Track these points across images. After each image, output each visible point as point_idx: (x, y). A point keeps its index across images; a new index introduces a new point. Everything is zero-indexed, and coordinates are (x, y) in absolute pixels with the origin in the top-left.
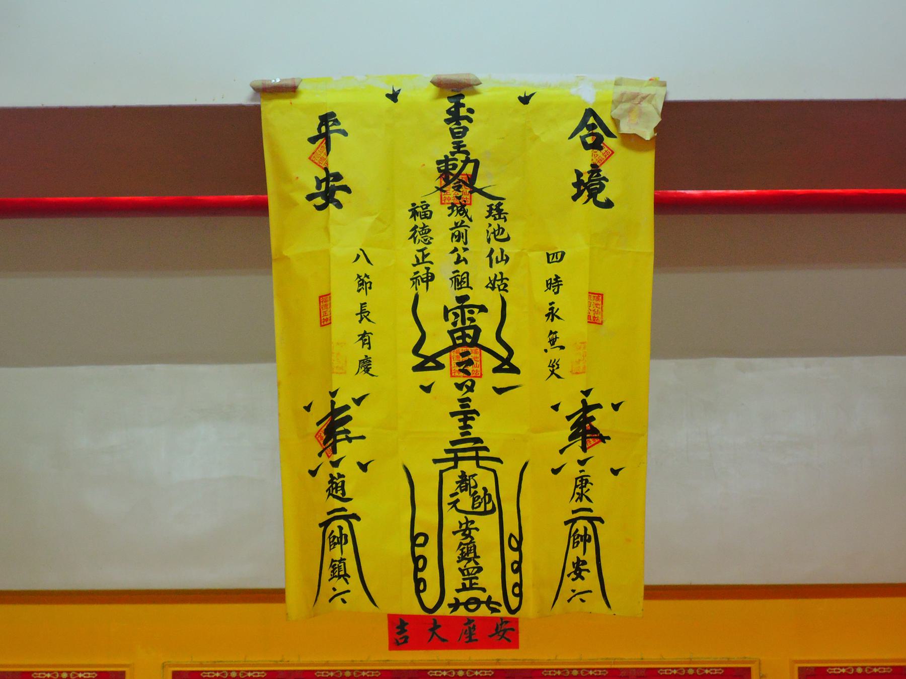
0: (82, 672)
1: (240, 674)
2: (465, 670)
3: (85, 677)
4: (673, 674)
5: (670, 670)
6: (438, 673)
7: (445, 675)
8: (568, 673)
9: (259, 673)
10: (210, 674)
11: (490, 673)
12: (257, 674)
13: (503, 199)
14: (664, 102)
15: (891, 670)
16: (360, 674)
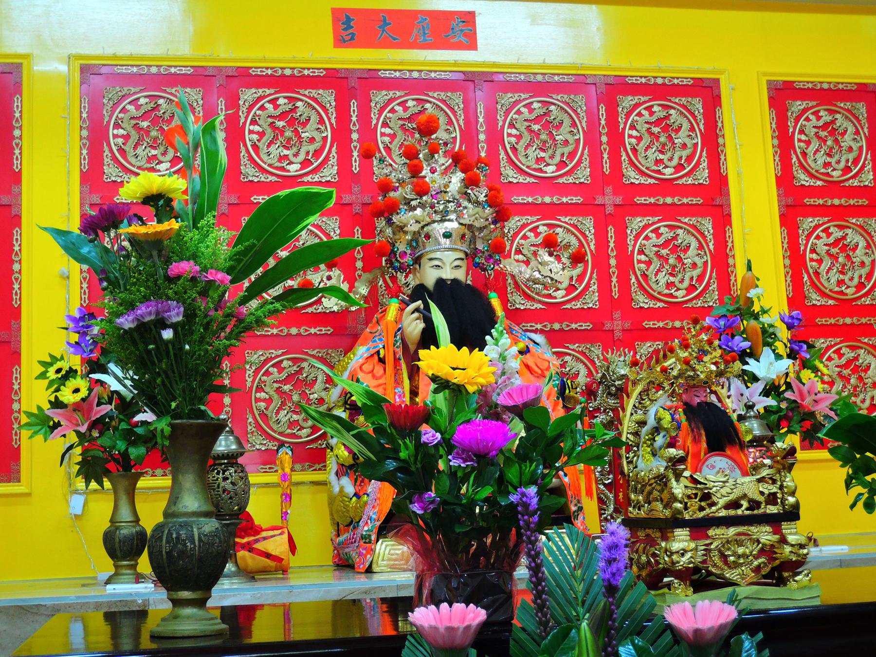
0: (175, 67)
1: (774, 135)
2: (159, 66)
3: (353, 159)
4: (567, 197)
5: (264, 70)
6: (85, 159)
7: (269, 73)
8: (85, 275)
9: (184, 69)
10: (729, 236)
11: (17, 167)
12: (85, 107)
13: (758, 72)
14: (81, 68)
15: (16, 306)
16: (302, 72)
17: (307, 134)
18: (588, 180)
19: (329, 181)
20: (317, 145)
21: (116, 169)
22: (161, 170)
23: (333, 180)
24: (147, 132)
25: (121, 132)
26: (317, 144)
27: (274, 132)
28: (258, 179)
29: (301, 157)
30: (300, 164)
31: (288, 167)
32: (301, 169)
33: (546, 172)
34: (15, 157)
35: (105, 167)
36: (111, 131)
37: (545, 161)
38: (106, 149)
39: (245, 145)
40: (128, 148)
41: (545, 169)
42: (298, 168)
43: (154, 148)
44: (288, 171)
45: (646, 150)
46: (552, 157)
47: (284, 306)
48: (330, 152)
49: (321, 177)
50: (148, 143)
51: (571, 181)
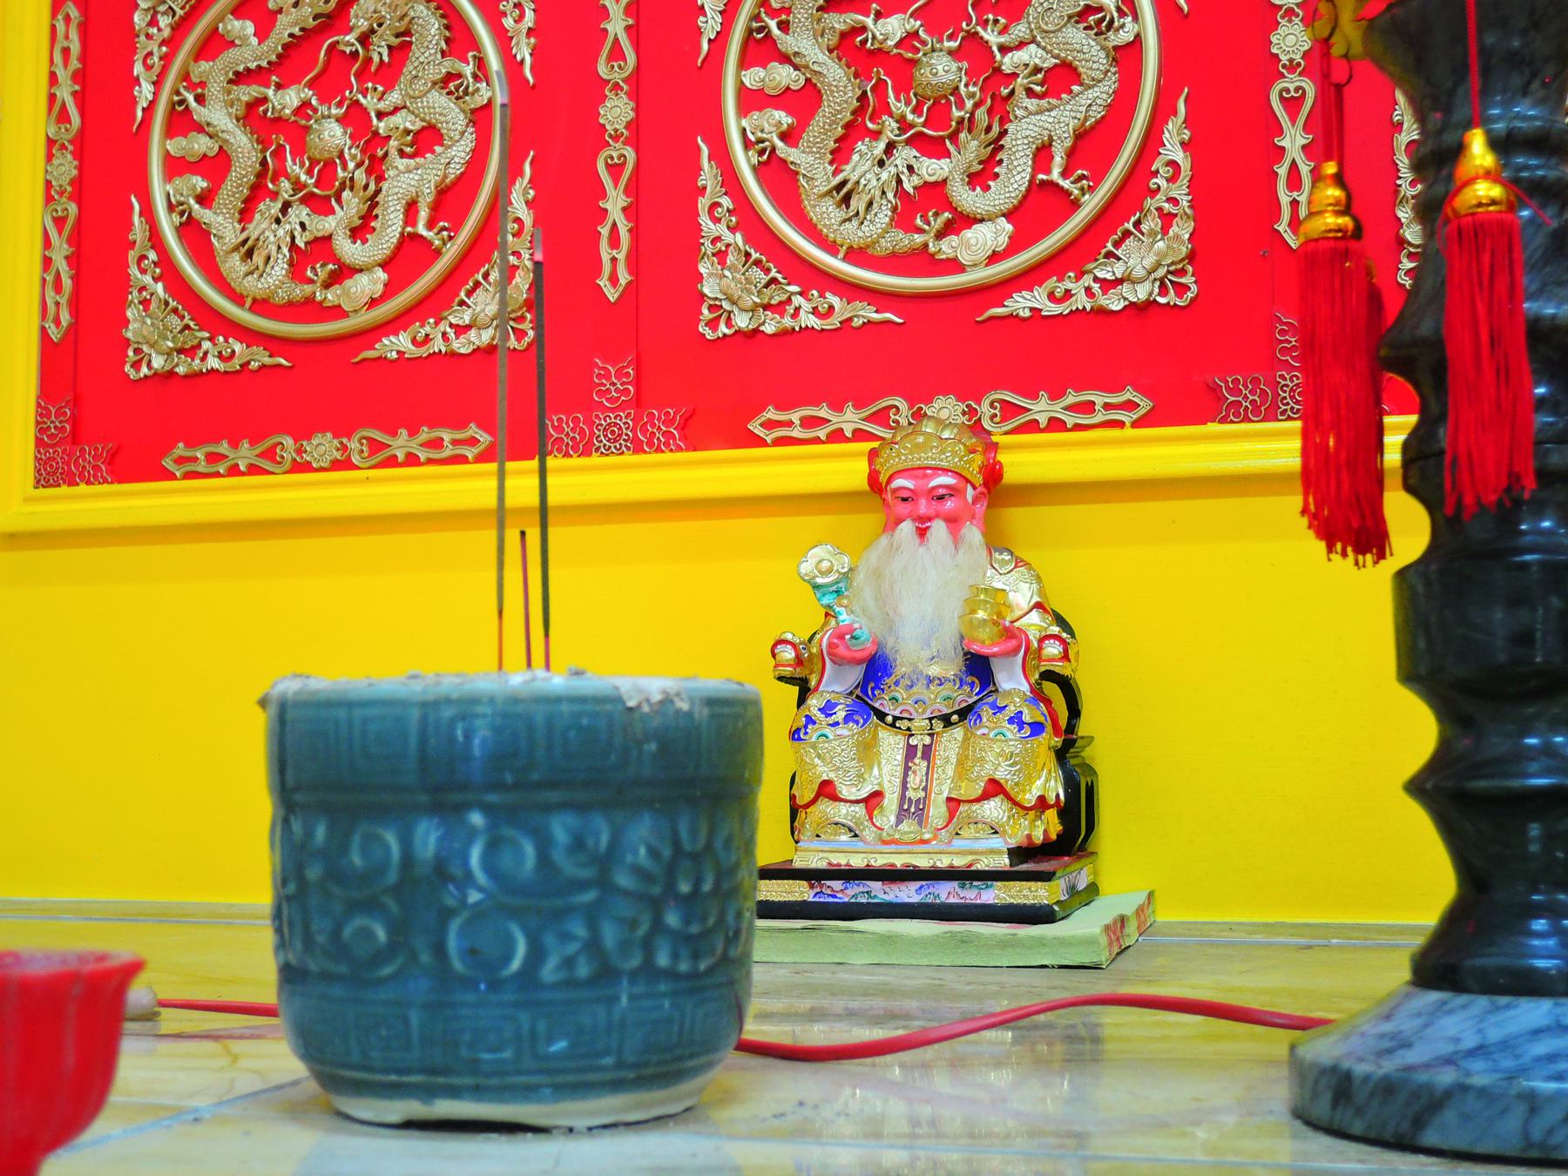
17: (1030, 55)
18: (1181, 289)
19: (1150, 304)
20: (1091, 101)
22: (964, 258)
23: (1171, 298)
24: (296, 130)
25: (782, 76)
27: (264, 143)
29: (1014, 179)
30: (1009, 215)
33: (954, 266)
34: (1282, 171)
36: (158, 147)
37: (332, 257)
38: (709, 175)
39: (722, 156)
40: (221, 224)
41: (947, 248)
43: (932, 147)
45: (246, 215)
46: (980, 178)
47: (813, 760)
48: (1152, 140)
50: (904, 125)
51: (1081, 301)
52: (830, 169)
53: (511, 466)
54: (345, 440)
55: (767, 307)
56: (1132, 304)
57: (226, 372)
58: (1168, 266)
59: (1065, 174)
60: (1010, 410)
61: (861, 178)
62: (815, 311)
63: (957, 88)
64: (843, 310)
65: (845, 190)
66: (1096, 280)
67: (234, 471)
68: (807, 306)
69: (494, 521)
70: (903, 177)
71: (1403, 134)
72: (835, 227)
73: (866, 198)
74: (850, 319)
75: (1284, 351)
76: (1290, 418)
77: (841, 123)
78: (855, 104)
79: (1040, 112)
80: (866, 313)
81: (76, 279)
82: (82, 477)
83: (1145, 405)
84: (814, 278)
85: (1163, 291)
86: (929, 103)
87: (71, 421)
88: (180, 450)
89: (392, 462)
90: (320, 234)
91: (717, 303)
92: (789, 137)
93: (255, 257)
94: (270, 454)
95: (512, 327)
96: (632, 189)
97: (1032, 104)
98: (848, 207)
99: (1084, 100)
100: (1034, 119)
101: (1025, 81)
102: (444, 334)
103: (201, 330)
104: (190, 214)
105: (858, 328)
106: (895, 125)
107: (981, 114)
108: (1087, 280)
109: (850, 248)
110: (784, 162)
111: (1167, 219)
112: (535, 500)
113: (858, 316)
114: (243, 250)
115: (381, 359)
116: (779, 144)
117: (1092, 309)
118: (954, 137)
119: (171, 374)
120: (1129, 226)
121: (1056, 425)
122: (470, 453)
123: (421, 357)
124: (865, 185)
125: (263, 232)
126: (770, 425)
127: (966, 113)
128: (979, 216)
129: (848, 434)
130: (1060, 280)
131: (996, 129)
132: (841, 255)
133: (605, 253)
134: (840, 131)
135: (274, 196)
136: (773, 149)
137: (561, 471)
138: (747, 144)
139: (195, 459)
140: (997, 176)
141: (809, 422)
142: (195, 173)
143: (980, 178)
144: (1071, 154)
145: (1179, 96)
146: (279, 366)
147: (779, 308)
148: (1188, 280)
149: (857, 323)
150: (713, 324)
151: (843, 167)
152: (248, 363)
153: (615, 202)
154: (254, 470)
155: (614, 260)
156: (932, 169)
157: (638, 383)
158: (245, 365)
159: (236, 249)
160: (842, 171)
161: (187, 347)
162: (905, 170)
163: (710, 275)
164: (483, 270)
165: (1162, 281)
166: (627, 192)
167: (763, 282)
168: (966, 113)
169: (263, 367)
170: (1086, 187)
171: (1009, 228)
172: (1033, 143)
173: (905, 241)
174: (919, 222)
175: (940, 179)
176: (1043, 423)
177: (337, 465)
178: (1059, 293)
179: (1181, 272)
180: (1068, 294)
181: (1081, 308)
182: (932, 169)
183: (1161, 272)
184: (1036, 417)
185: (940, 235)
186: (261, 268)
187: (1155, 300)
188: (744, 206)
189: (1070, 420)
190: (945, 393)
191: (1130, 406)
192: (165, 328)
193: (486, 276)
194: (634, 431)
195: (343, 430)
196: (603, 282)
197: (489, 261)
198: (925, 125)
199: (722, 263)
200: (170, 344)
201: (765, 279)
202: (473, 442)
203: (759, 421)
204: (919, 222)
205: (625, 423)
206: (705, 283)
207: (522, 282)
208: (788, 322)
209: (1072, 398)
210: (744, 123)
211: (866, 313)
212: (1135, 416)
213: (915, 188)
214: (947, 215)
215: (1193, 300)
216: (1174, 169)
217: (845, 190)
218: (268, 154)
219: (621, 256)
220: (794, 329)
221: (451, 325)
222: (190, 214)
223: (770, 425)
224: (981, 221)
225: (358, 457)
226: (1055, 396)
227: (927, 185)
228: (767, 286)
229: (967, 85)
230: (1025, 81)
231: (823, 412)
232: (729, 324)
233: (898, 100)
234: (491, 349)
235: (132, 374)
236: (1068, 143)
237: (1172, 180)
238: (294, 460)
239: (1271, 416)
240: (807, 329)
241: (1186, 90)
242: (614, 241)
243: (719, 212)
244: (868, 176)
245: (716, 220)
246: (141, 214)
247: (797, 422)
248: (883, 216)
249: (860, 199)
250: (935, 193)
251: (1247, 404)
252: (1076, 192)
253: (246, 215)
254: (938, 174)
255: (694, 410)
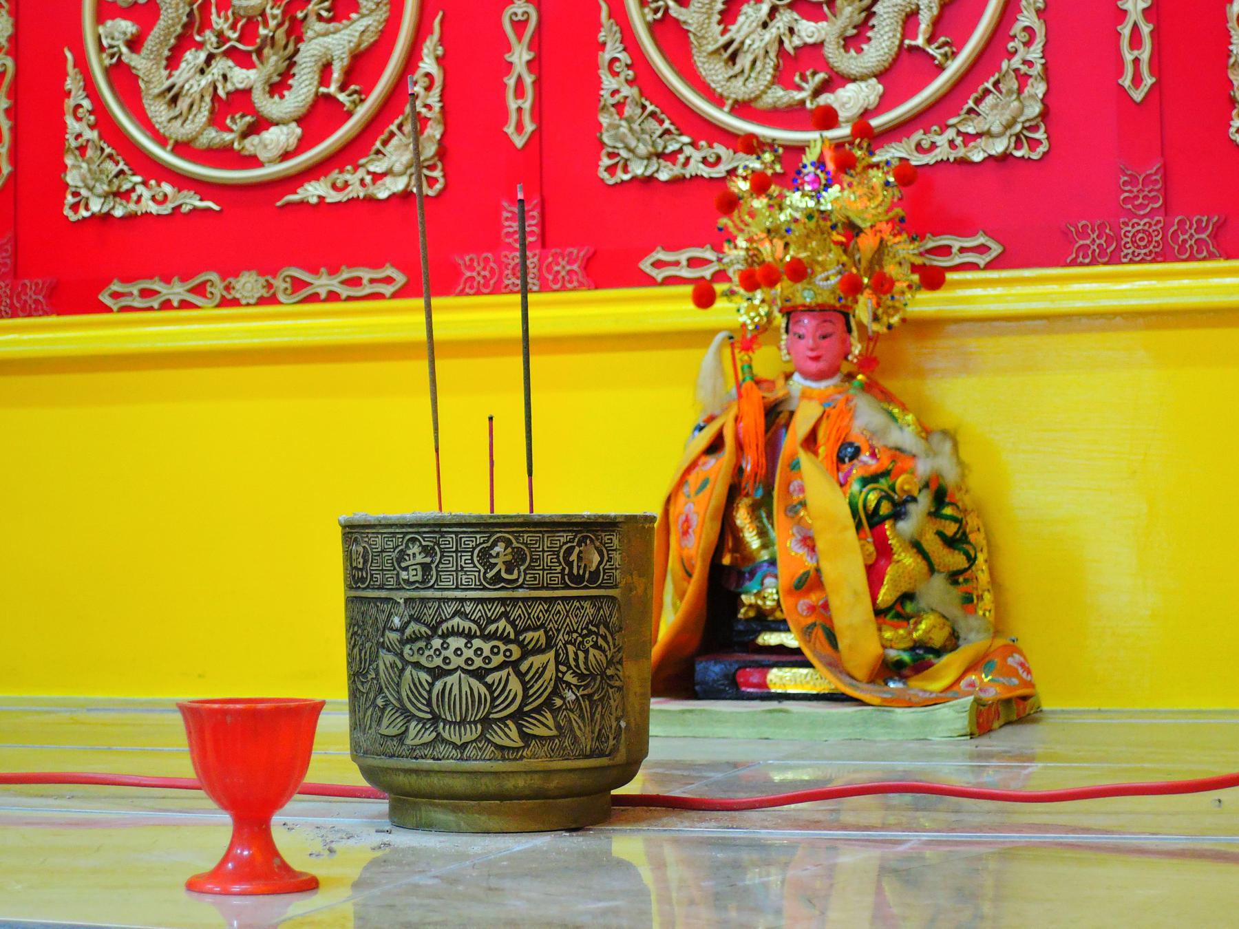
19: (1006, 157)
21: (652, 124)
22: (263, 156)
26: (365, 22)
28: (677, 170)
29: (302, 91)
31: (251, 145)
32: (304, 145)
35: (604, 120)
41: (251, 145)
42: (293, 142)
43: (243, 60)
44: (253, 161)
49: (968, 138)
51: (356, 191)
52: (165, 73)
53: (436, 301)
54: (269, 278)
55: (661, 156)
56: (990, 156)
57: (711, 179)
58: (1023, 123)
59: (343, 88)
60: (298, 284)
61: (746, 38)
62: (705, 161)
63: (264, 10)
64: (175, 198)
65: (730, 50)
66: (959, 133)
67: (166, 305)
68: (146, 194)
69: (426, 353)
70: (783, 38)
71: (71, 99)
72: (723, 83)
73: (750, 57)
74: (180, 206)
75: (509, 235)
76: (512, 292)
77: (174, 35)
78: (185, 19)
79: (326, 34)
80: (192, 201)
81: (537, 84)
82: (23, 309)
83: (996, 249)
84: (153, 170)
85: (1018, 146)
86: (244, 21)
87: (1163, 190)
88: (116, 286)
89: (314, 298)
90: (240, 86)
91: (616, 151)
92: (135, 44)
93: (179, 103)
94: (200, 290)
95: (425, 176)
96: (535, 45)
97: (320, 27)
98: (734, 64)
99: (360, 25)
100: (321, 40)
101: (317, 7)
102: (362, 181)
103: (134, 174)
104: (119, 58)
105: (184, 214)
106: (214, 39)
107: (280, 34)
108: (361, 173)
109: (736, 101)
110: (676, 21)
111: (1023, 79)
112: (518, 331)
113: (186, 204)
114: (726, 55)
115: (303, 204)
116: (124, 50)
117: (955, 159)
118: (259, 52)
119: (108, 216)
120: (989, 85)
121: (333, 297)
122: (388, 290)
123: (927, 164)
124: (750, 45)
125: (187, 81)
126: (116, 295)
127: (270, 31)
128: (852, 77)
129: (175, 304)
130: (341, 171)
131: (291, 47)
132: (169, 148)
133: (513, 104)
134: (173, 41)
135: (200, 46)
136: (667, 8)
137: (539, 304)
138: (101, 48)
139: (131, 294)
140: (869, 39)
141: (146, 293)
142: (125, 18)
143: (278, 87)
144: (937, 23)
145: (434, 18)
146: (209, 210)
147: (672, 157)
148: (1040, 135)
149: (185, 209)
150: (1033, 144)
151: (731, 27)
152: (180, 206)
153: (520, 56)
154: (185, 305)
155: (520, 110)
156: (241, 77)
157: (1165, 191)
158: (177, 209)
159: (162, 94)
160: (729, 30)
161: (667, 151)
162: (787, 32)
163: (73, 166)
164: (397, 122)
165: (1018, 136)
166: (530, 48)
167: (114, 173)
168: (270, 31)
169: (195, 210)
170: (949, 54)
171: (299, 131)
172: (903, 11)
173: (213, 137)
174: (228, 121)
175: (819, 40)
176: (323, 296)
177: (262, 301)
178: (339, 184)
179: (1035, 128)
180: (346, 184)
181: (945, 159)
182: (241, 77)
183: (1018, 128)
184: (318, 290)
185: (244, 135)
186: (747, 71)
187: (1011, 154)
188: (100, 109)
189: (344, 292)
190: (249, 269)
191: (983, 249)
192: (102, 172)
193: (400, 127)
194: (11, 298)
195: (268, 269)
196: (510, 129)
197: (402, 112)
198: (239, 40)
199: (83, 154)
200: (106, 187)
201: (115, 170)
202: (389, 280)
203: (109, 292)
204: (797, 79)
205: (1133, 226)
206: (68, 172)
207: (434, 131)
208: (132, 207)
209: (346, 274)
210: (101, 30)
211: (192, 201)
212: (987, 258)
213: (228, 94)
214: (249, 119)
215: (1045, 154)
216: (1030, 36)
217: (730, 50)
218: (195, 6)
219: (527, 105)
220: (136, 214)
221: (369, 173)
222: (119, 58)
223: (658, 264)
224: (277, 124)
225: (285, 297)
226: (333, 271)
227: (237, 91)
228: (117, 176)
229: (272, 8)
230: (317, 7)
231: (156, 285)
232: (87, 208)
233: (219, 16)
234: (406, 195)
235: (1042, 149)
236: (346, 62)
237: (428, 89)
238: (223, 297)
239: (496, 290)
240: (147, 215)
241: (441, 14)
242: (520, 92)
243: (617, 67)
244: (191, 82)
245: (79, 119)
246: (610, 16)
247: (684, 263)
248: (203, 115)
249: (183, 102)
250: (241, 98)
251: (1095, 247)
252: (939, 57)
253: (173, 62)
254: (816, 36)
255: (595, 253)
